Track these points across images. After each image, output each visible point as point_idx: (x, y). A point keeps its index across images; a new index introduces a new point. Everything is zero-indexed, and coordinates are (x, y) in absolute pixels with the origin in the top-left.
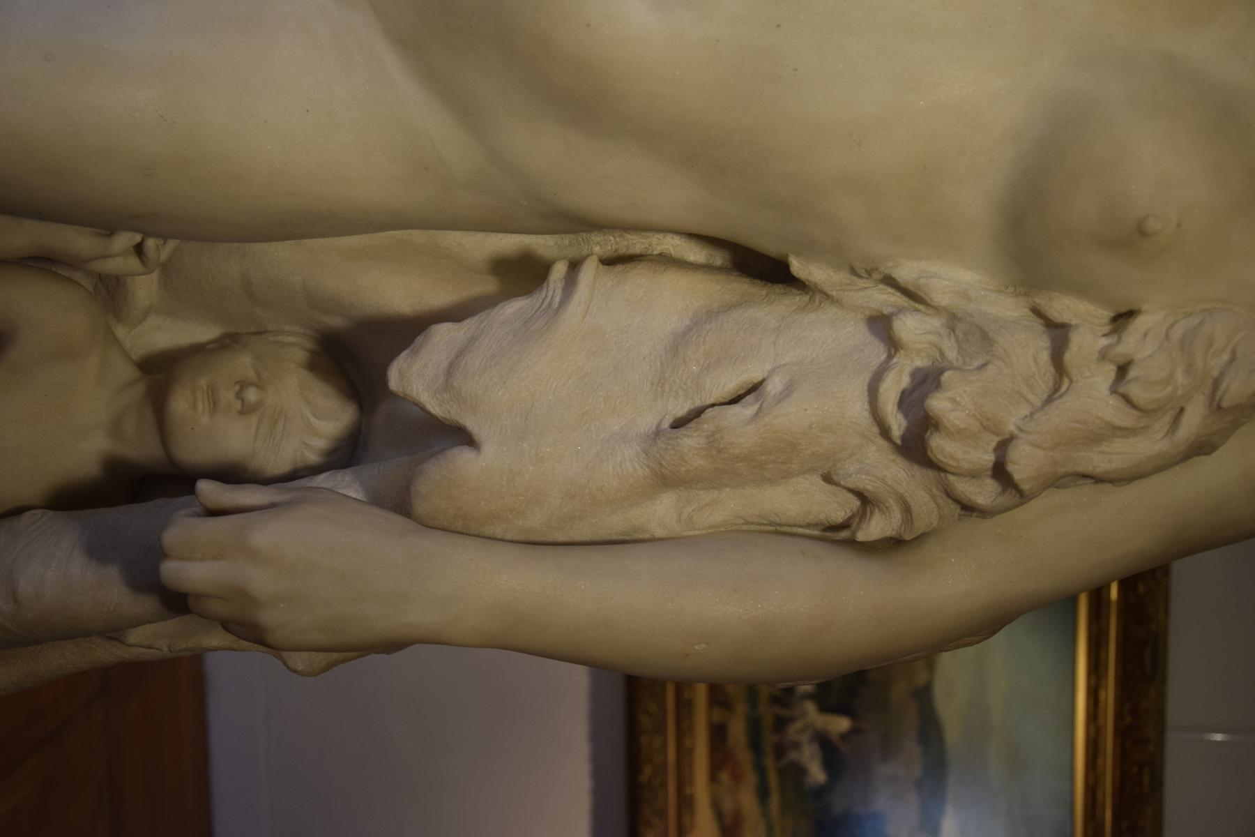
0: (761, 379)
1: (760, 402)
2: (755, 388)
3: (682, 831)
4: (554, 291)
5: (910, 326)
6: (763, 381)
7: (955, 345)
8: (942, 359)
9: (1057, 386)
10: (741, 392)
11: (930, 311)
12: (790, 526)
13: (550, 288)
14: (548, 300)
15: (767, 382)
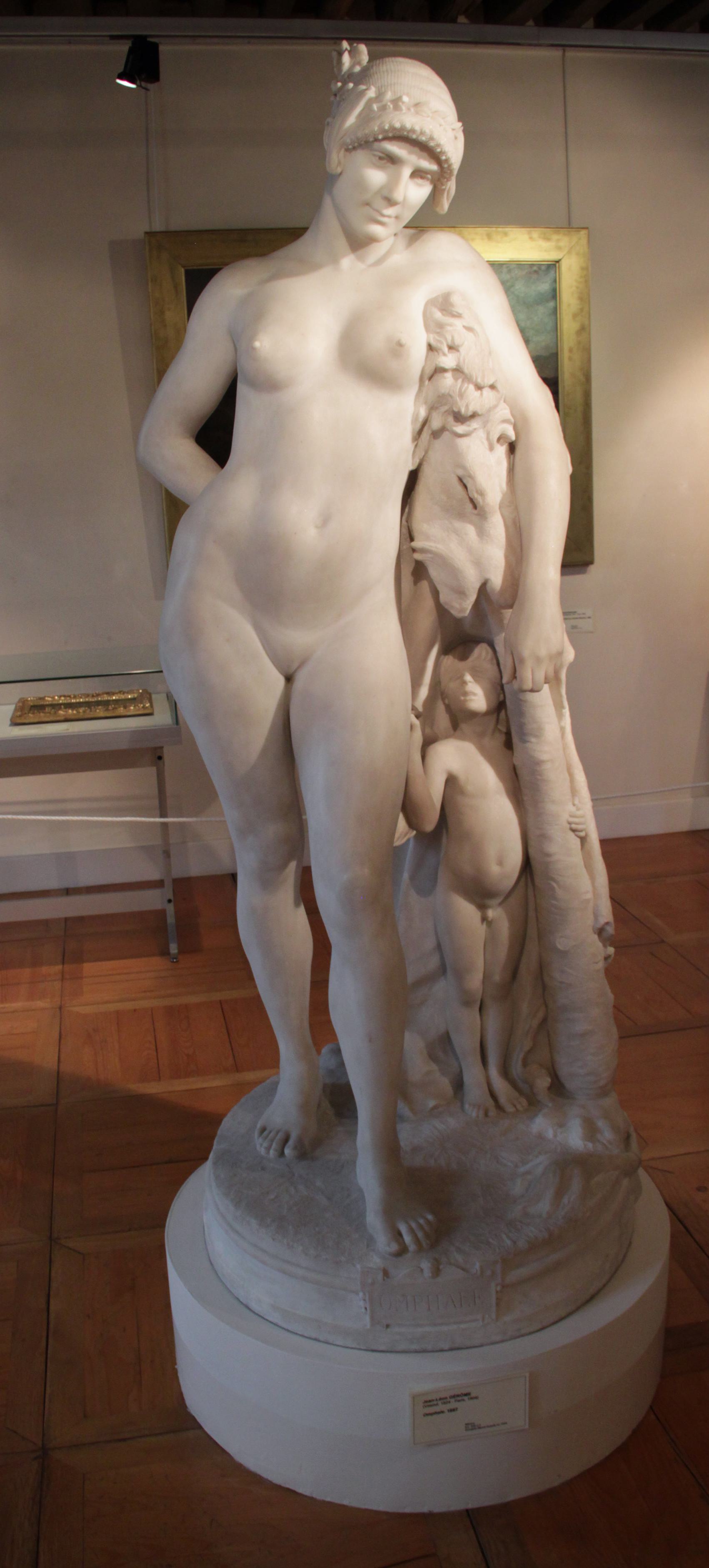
2: (460, 480)
5: (436, 423)
10: (462, 484)
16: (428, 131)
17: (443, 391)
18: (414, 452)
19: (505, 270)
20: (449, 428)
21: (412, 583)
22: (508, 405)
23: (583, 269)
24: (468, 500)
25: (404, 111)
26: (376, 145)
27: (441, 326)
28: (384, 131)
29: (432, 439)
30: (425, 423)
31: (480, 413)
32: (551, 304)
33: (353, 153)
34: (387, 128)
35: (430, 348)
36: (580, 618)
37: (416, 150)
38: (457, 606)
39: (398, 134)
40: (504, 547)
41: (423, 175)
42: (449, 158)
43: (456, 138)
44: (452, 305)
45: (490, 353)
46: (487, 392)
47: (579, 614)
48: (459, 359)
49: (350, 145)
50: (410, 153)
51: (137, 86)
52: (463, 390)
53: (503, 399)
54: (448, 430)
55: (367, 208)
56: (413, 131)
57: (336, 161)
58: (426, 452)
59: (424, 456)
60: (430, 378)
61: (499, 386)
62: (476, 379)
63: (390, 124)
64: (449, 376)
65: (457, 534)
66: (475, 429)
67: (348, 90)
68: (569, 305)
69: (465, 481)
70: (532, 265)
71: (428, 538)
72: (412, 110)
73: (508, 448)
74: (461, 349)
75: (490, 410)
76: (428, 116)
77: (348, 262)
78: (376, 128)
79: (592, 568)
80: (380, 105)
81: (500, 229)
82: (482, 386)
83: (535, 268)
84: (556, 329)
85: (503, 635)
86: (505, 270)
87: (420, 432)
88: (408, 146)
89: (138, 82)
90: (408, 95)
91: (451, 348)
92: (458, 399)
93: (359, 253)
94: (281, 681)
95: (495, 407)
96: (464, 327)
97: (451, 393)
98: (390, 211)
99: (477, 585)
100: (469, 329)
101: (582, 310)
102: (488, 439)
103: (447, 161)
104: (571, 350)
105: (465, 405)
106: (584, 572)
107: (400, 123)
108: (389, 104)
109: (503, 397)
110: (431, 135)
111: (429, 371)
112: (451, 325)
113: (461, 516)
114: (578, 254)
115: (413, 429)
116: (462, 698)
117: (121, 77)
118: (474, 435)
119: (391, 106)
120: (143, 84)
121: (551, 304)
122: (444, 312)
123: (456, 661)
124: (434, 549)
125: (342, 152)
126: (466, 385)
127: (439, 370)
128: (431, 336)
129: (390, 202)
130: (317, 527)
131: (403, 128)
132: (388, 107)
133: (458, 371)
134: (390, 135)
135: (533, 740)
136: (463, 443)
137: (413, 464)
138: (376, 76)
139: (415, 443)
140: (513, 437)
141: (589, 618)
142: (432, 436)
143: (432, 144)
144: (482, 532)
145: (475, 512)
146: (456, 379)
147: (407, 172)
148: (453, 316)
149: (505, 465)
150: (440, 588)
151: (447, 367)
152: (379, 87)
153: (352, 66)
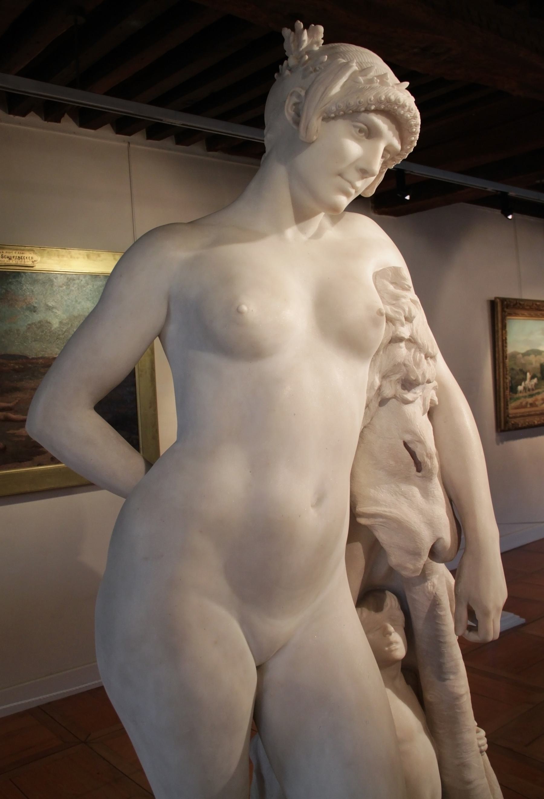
17: (400, 360)
28: (380, 102)
33: (332, 122)
38: (410, 566)
48: (412, 330)
55: (339, 179)
63: (386, 97)
64: (403, 344)
65: (405, 497)
67: (322, 63)
71: (376, 502)
77: (291, 232)
80: (365, 78)
93: (302, 224)
97: (407, 362)
108: (375, 78)
113: (407, 480)
116: (387, 649)
123: (373, 613)
124: (388, 514)
127: (396, 340)
135: (452, 677)
146: (409, 349)
153: (311, 45)
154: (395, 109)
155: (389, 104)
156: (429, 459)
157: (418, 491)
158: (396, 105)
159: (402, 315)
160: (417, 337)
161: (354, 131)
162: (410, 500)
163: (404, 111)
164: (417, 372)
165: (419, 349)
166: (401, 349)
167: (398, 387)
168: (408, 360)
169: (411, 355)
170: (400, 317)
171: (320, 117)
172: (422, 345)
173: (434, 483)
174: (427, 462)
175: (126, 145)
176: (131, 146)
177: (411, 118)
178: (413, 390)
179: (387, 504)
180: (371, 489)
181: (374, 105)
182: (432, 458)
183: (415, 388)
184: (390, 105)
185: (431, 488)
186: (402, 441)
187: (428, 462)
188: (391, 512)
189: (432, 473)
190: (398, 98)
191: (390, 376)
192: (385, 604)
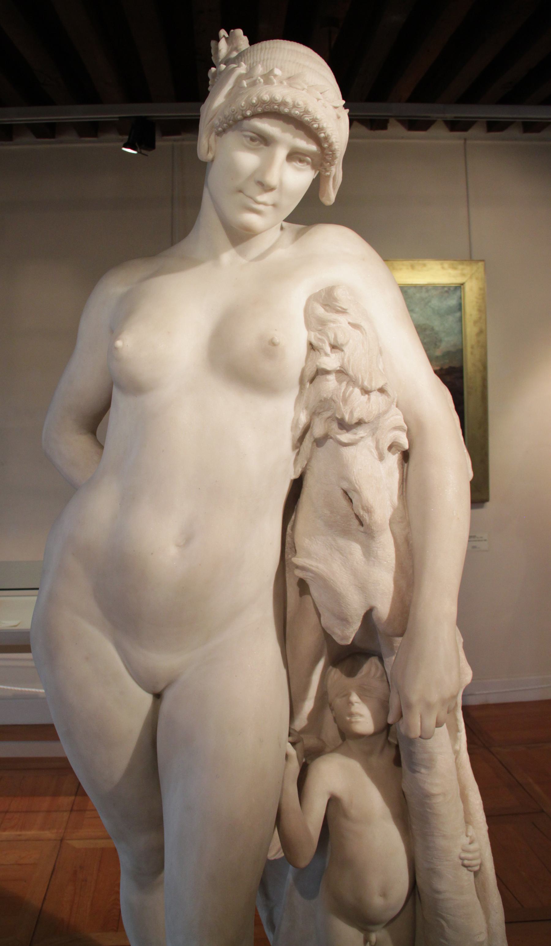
0: (342, 490)
1: (351, 491)
2: (346, 493)
3: (550, 119)
4: (307, 576)
5: (318, 430)
6: (342, 489)
7: (326, 412)
8: (331, 417)
9: (341, 372)
10: (348, 498)
11: (312, 423)
12: (403, 475)
13: (306, 577)
14: (310, 578)
15: (343, 488)
16: (301, 103)
18: (296, 460)
19: (424, 290)
20: (332, 436)
21: (298, 594)
22: (401, 410)
23: (480, 289)
24: (354, 516)
25: (276, 84)
26: (246, 122)
27: (323, 322)
29: (315, 447)
30: (307, 429)
31: (366, 420)
32: (458, 314)
33: (224, 135)
34: (254, 101)
35: (312, 347)
36: (479, 541)
37: (291, 127)
39: (268, 109)
40: (394, 570)
41: (302, 157)
42: (328, 136)
43: (339, 117)
44: (335, 300)
45: (381, 352)
46: (375, 396)
47: (478, 538)
49: (219, 126)
50: (284, 131)
51: (138, 152)
52: (347, 394)
53: (395, 404)
54: (331, 438)
55: (241, 195)
56: (284, 103)
57: (206, 146)
58: (309, 460)
59: (307, 465)
60: (312, 381)
61: (389, 389)
62: (363, 382)
63: (258, 98)
64: (332, 378)
65: (341, 553)
66: (362, 438)
68: (471, 315)
69: (350, 495)
70: (443, 287)
71: (309, 555)
72: (285, 83)
73: (401, 455)
74: (345, 349)
75: (378, 417)
76: (303, 89)
78: (243, 104)
79: (488, 504)
80: (249, 81)
81: (420, 262)
82: (369, 389)
83: (446, 289)
84: (461, 332)
85: (393, 658)
86: (424, 290)
87: (301, 439)
88: (281, 123)
89: (139, 149)
90: (281, 68)
91: (334, 347)
92: (341, 404)
93: (241, 247)
94: (148, 699)
95: (386, 412)
96: (349, 323)
97: (335, 398)
98: (265, 198)
99: (362, 612)
100: (355, 326)
101: (480, 318)
102: (377, 448)
103: (326, 139)
104: (472, 347)
105: (349, 411)
106: (482, 507)
107: (269, 95)
108: (259, 78)
109: (395, 400)
110: (305, 108)
111: (310, 373)
112: (334, 322)
113: (346, 533)
114: (477, 279)
115: (293, 436)
117: (125, 146)
118: (361, 443)
119: (262, 80)
120: (143, 151)
121: (458, 314)
122: (327, 308)
123: (344, 677)
124: (314, 569)
125: (213, 137)
126: (351, 389)
127: (321, 372)
128: (312, 334)
129: (266, 188)
130: (178, 546)
131: (273, 101)
132: (258, 81)
133: (342, 372)
134: (259, 110)
136: (347, 452)
137: (295, 472)
138: (249, 55)
139: (297, 450)
140: (405, 444)
141: (485, 540)
142: (315, 444)
143: (307, 118)
144: (368, 552)
145: (362, 529)
146: (340, 382)
147: (281, 153)
148: (338, 312)
149: (397, 476)
150: (321, 610)
151: (329, 369)
152: (250, 64)
153: (229, 53)
154: (277, 109)
155: (266, 105)
156: (366, 512)
157: (360, 548)
158: (274, 105)
159: (324, 343)
160: (348, 367)
161: (246, 141)
162: (346, 557)
163: (288, 108)
164: (343, 410)
165: (353, 382)
166: (327, 383)
167: (335, 425)
168: (337, 395)
169: (340, 389)
170: (323, 345)
171: (211, 133)
172: (354, 377)
173: (378, 542)
174: (364, 516)
175: (462, 142)
176: (468, 142)
177: (302, 114)
178: (355, 430)
179: (318, 558)
180: (306, 539)
181: (248, 110)
182: (371, 513)
183: (356, 428)
184: (267, 105)
185: (374, 547)
186: (339, 488)
187: (365, 516)
188: (317, 568)
189: (372, 529)
190: (273, 96)
191: (321, 413)
192: (361, 671)
